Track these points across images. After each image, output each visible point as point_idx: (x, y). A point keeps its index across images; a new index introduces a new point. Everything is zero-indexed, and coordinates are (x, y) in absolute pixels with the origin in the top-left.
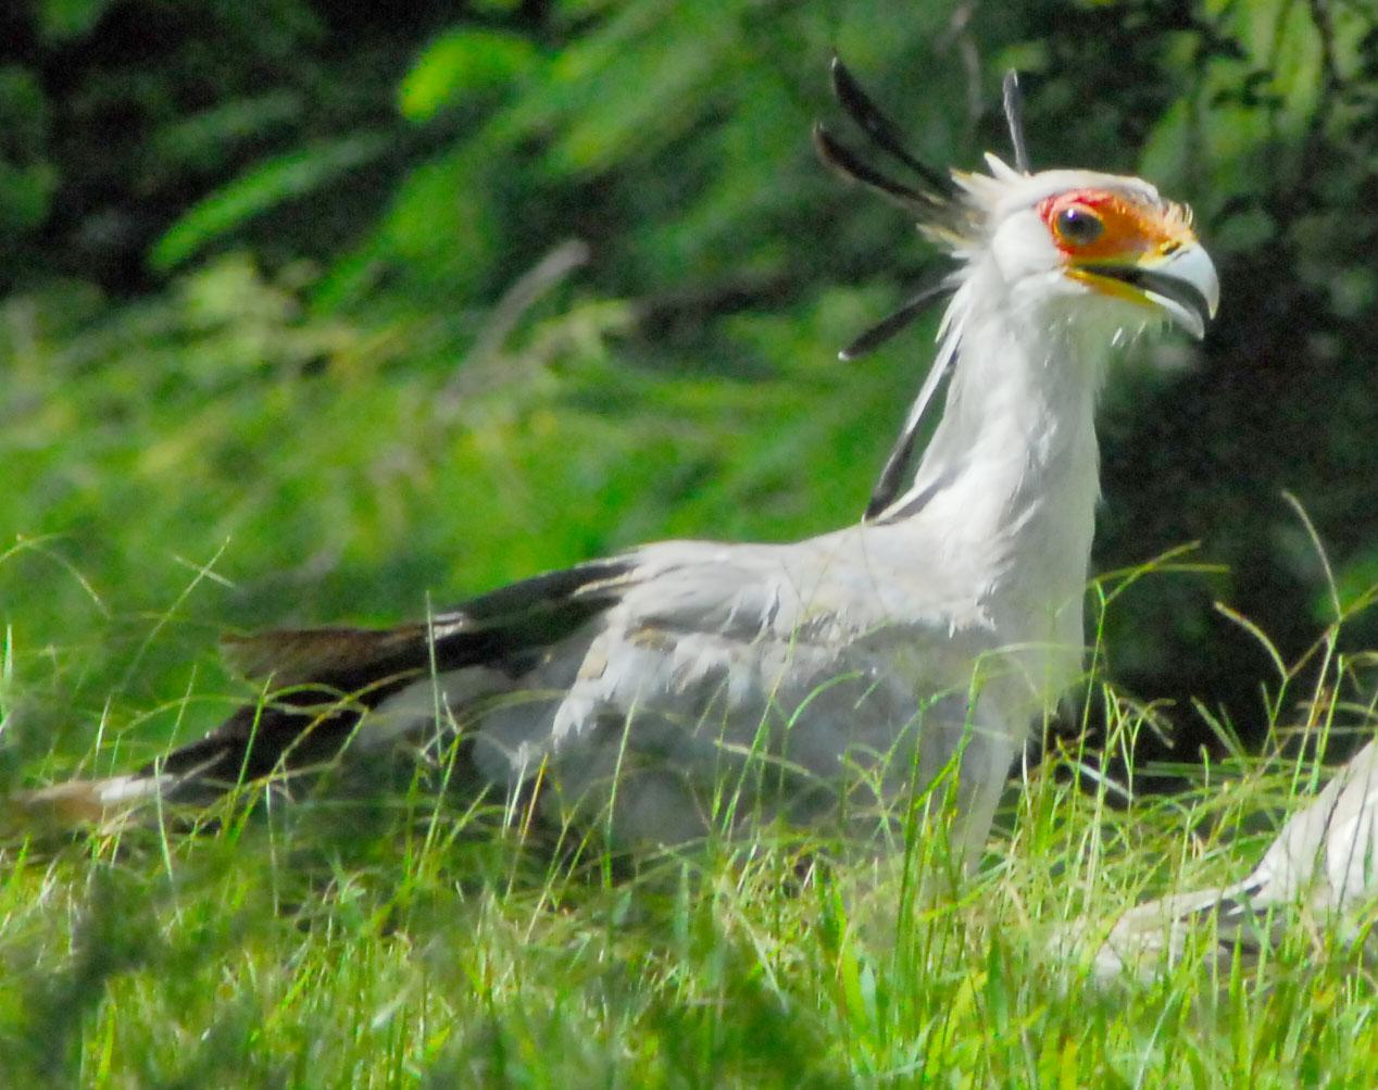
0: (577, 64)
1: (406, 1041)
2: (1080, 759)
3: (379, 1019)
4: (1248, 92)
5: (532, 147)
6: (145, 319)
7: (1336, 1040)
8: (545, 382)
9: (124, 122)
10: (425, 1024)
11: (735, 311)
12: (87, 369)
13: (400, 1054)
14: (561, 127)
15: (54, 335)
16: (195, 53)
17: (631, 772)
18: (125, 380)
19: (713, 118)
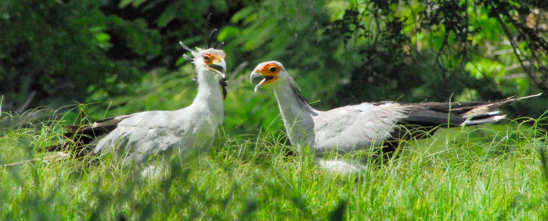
0: (247, 32)
1: (221, 192)
2: (448, 127)
3: (217, 188)
4: (124, 145)
5: (240, 46)
6: (174, 74)
7: (377, 193)
8: (241, 84)
9: (174, 40)
10: (292, 185)
11: (124, 142)
12: (165, 82)
13: (221, 194)
14: (244, 43)
15: (160, 76)
16: (185, 27)
17: (489, 101)
18: (173, 83)
19: (270, 41)
